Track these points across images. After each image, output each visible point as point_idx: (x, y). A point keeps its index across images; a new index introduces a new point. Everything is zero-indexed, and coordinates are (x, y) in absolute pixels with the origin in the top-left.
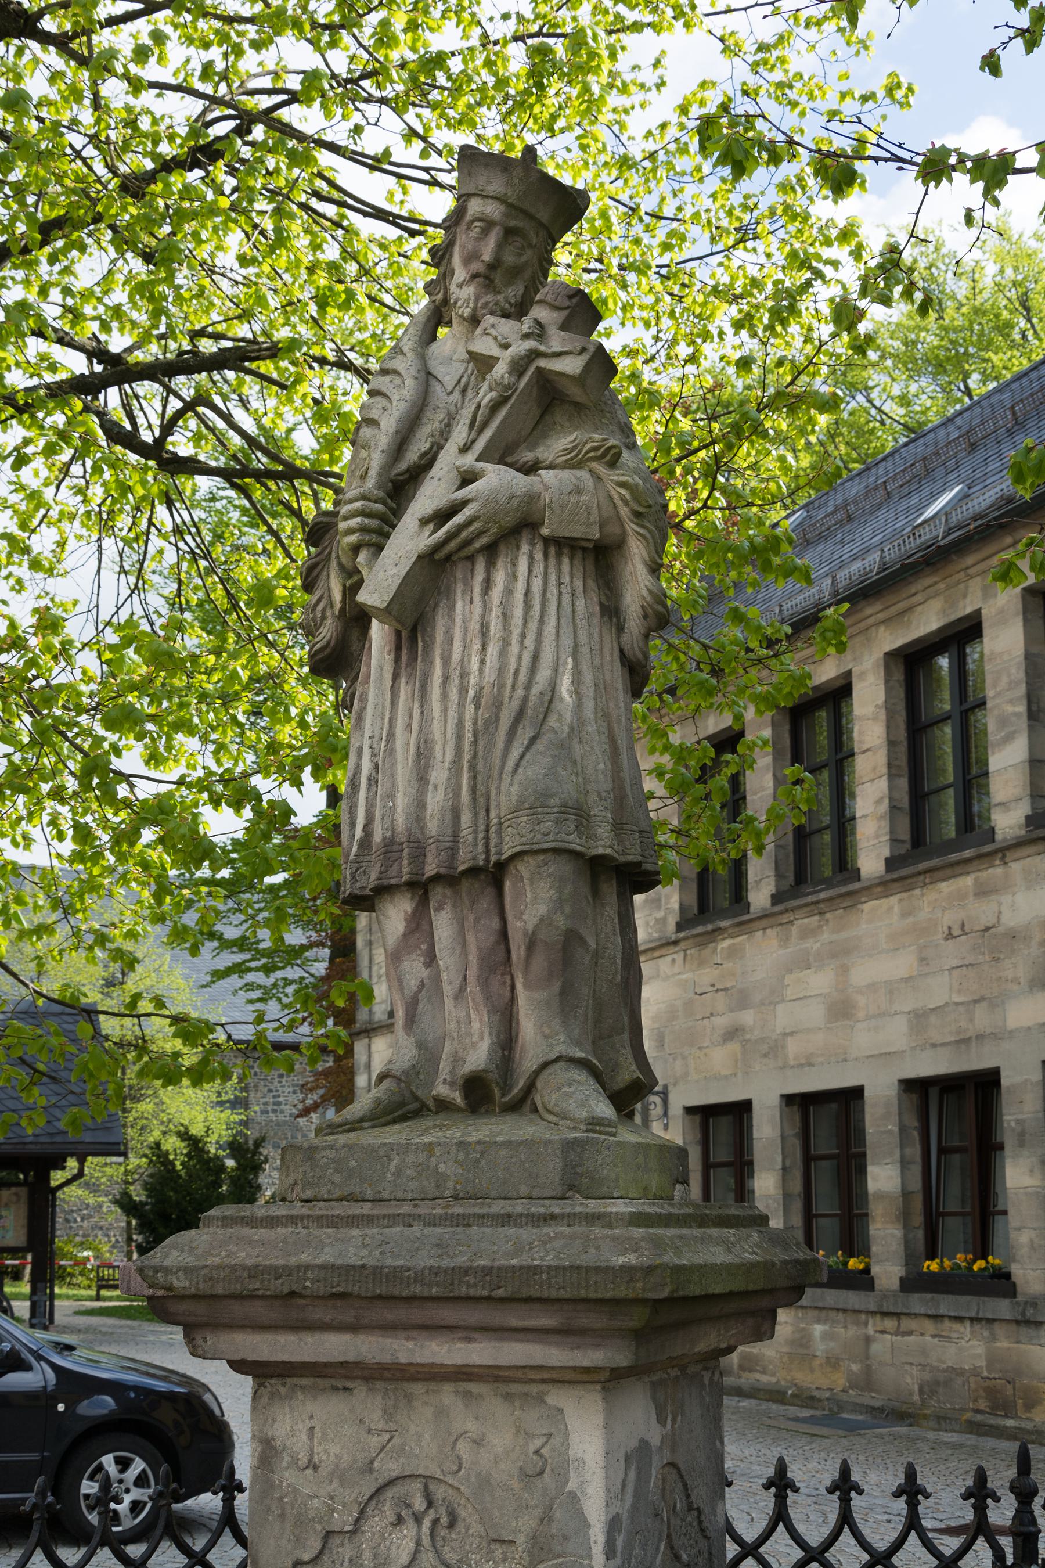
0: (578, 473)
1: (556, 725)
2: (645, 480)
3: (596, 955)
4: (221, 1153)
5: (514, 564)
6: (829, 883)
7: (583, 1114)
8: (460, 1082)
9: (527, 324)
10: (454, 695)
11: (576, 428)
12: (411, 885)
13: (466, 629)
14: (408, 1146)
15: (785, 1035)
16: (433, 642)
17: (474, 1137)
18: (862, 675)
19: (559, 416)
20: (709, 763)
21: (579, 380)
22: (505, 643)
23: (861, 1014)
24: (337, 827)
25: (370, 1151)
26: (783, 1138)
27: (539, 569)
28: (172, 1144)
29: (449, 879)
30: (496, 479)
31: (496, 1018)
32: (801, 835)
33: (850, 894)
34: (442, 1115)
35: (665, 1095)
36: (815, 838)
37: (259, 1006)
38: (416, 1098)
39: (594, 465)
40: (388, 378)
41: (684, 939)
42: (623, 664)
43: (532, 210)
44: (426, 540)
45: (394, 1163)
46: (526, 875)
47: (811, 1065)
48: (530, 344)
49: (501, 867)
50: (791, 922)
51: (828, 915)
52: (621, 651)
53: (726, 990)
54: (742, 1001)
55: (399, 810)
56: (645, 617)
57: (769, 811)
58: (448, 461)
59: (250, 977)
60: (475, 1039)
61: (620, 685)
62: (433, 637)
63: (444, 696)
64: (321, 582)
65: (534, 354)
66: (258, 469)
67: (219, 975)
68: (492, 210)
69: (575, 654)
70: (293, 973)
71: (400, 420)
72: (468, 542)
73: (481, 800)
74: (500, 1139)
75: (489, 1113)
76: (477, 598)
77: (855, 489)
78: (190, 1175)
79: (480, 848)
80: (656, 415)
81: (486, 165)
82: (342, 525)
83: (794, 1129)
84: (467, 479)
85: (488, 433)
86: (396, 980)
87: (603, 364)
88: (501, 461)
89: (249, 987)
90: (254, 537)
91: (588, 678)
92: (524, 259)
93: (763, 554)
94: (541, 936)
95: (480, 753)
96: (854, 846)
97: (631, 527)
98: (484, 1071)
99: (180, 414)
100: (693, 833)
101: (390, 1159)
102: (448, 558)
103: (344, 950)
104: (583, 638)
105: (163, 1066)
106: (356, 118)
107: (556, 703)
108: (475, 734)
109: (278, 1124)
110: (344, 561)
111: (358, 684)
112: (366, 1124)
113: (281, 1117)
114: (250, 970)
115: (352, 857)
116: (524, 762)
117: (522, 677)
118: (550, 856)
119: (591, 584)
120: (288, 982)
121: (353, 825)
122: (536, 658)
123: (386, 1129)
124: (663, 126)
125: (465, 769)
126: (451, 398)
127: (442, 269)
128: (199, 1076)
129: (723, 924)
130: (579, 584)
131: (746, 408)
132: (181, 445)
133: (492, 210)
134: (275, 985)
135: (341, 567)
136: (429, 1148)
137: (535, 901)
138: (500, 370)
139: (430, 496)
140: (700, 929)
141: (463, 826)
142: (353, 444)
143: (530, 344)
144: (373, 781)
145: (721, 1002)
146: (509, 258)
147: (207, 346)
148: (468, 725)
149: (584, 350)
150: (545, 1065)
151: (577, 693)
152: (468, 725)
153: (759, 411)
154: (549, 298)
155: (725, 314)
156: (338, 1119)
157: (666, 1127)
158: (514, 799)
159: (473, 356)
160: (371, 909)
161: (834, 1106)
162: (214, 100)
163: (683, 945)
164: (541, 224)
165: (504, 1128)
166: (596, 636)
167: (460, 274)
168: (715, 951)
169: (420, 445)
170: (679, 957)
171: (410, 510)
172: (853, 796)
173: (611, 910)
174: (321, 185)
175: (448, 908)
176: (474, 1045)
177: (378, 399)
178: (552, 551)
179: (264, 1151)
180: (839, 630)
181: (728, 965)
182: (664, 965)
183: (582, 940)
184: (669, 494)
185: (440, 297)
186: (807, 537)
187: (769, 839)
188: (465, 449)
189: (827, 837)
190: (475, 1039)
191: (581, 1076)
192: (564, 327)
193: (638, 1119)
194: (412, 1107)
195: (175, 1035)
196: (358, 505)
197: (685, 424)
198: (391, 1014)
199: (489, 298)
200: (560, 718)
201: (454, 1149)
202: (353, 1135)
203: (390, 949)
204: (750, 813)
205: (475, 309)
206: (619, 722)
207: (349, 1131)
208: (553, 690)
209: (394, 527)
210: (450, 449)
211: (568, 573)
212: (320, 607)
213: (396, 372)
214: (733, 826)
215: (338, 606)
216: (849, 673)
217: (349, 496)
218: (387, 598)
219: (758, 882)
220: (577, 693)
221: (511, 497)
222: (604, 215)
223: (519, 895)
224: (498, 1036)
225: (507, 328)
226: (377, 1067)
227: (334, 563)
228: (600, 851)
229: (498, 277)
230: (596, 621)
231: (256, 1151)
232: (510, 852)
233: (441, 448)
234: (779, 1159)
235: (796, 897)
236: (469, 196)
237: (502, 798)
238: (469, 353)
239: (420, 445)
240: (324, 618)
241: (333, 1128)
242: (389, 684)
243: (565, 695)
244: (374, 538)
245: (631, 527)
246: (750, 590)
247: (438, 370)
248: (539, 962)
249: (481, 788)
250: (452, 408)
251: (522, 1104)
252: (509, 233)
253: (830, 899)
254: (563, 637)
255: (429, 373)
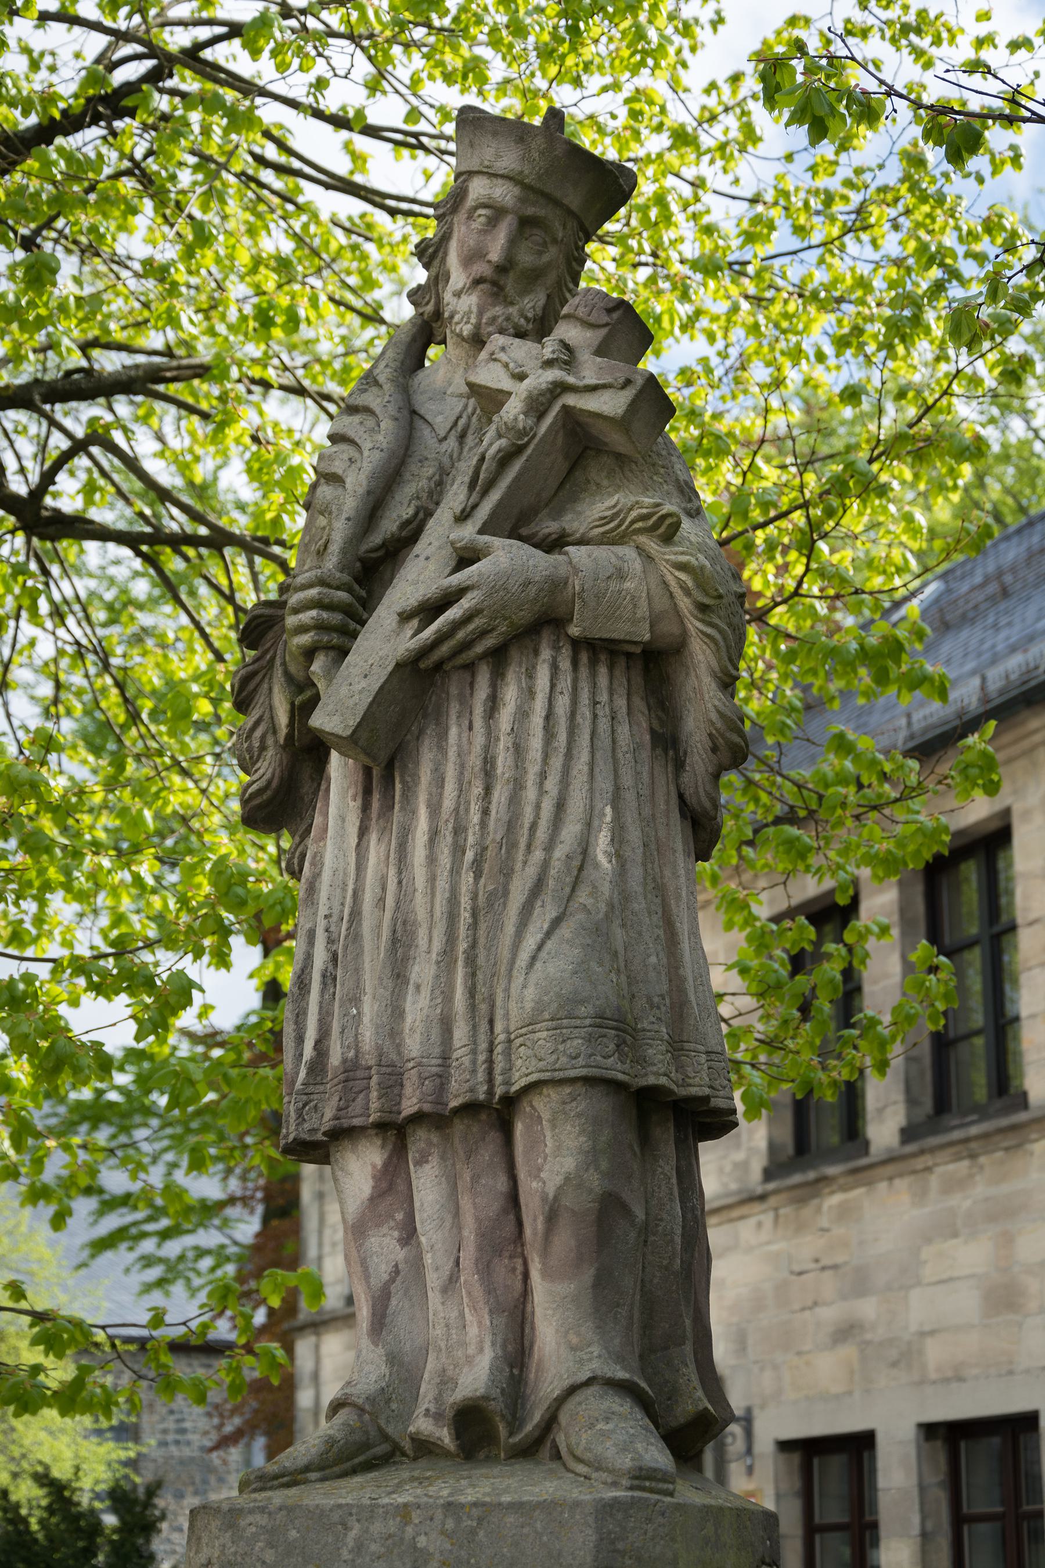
0: (620, 550)
1: (589, 902)
2: (713, 560)
3: (646, 1230)
4: (97, 1505)
5: (531, 675)
6: (983, 1113)
7: (626, 1462)
8: (449, 1413)
9: (549, 348)
10: (445, 858)
11: (618, 488)
12: (382, 1127)
13: (462, 766)
14: (373, 1508)
15: (923, 1334)
16: (416, 783)
17: (469, 1496)
18: (1027, 814)
19: (595, 472)
20: (809, 948)
21: (623, 423)
22: (518, 785)
23: (1033, 1305)
24: (276, 1037)
25: (319, 1515)
26: (922, 1488)
27: (565, 682)
28: (27, 1493)
29: (436, 1119)
30: (506, 558)
31: (502, 1320)
32: (943, 1045)
33: (1014, 1128)
34: (423, 1462)
35: (747, 1421)
36: (963, 1048)
37: (156, 1298)
38: (385, 1437)
39: (642, 539)
40: (356, 419)
41: (775, 1192)
42: (683, 816)
43: (558, 194)
44: (408, 641)
45: (353, 1534)
46: (546, 1115)
47: (960, 1379)
48: (553, 374)
49: (510, 1103)
50: (928, 1169)
51: (982, 1160)
52: (681, 796)
53: (835, 1267)
54: (859, 1284)
55: (366, 1020)
56: (714, 749)
57: (896, 1010)
58: (440, 534)
59: (148, 1246)
60: (471, 1351)
61: (679, 846)
62: (416, 777)
63: (432, 860)
64: (261, 698)
65: (560, 388)
66: (176, 538)
67: (103, 1244)
68: (503, 193)
69: (616, 801)
70: (209, 1238)
71: (372, 477)
72: (466, 645)
73: (483, 1010)
74: (506, 1499)
75: (491, 1459)
76: (478, 723)
77: (1012, 553)
78: (50, 1538)
79: (481, 1076)
80: (727, 464)
81: (495, 134)
82: (291, 621)
83: (937, 1476)
84: (465, 558)
85: (495, 496)
86: (359, 1263)
87: (654, 402)
88: (514, 534)
89: (148, 1261)
90: (168, 620)
91: (634, 835)
92: (546, 258)
93: (883, 659)
94: (566, 1202)
95: (482, 941)
96: (1018, 1054)
97: (694, 625)
98: (485, 1398)
99: (66, 457)
100: (790, 1044)
101: (346, 1528)
102: (439, 666)
103: (282, 1208)
104: (627, 779)
105: (16, 1385)
106: (320, 68)
107: (589, 872)
108: (474, 914)
109: (182, 1462)
110: (293, 669)
111: (309, 841)
112: (313, 1476)
113: (187, 1452)
114: (144, 1235)
115: (298, 1085)
116: (543, 955)
117: (542, 834)
118: (580, 1088)
119: (639, 703)
120: (201, 1253)
121: (300, 1039)
122: (560, 806)
123: (342, 1482)
124: (735, 79)
125: (460, 963)
126: (445, 446)
127: (434, 271)
128: (70, 1399)
129: (831, 1170)
130: (621, 703)
131: (852, 457)
132: (67, 496)
133: (503, 193)
134: (181, 1258)
135: (288, 675)
136: (404, 1511)
137: (556, 1153)
138: (513, 409)
139: (418, 578)
140: (797, 1178)
141: (457, 1043)
142: (307, 507)
143: (553, 374)
144: (329, 979)
145: (829, 1284)
146: (526, 258)
147: (110, 362)
148: (465, 901)
149: (628, 382)
150: (572, 1390)
151: (618, 855)
152: (465, 901)
153: (871, 461)
154: (581, 312)
155: (820, 328)
156: (273, 1468)
157: (750, 1470)
158: (529, 1005)
159: (475, 389)
160: (324, 1159)
161: (996, 1441)
162: (121, 37)
163: (773, 1201)
164: (570, 212)
165: (513, 1482)
166: (646, 777)
167: (458, 278)
168: (819, 1210)
169: (400, 510)
170: (768, 1219)
171: (385, 601)
172: (1015, 982)
173: (667, 1166)
174: (271, 152)
175: (434, 1160)
176: (469, 1360)
177: (343, 447)
178: (584, 657)
179: (160, 1502)
180: (988, 764)
181: (839, 1231)
182: (746, 1230)
183: (625, 1210)
184: (746, 574)
185: (430, 308)
186: (944, 619)
187: (896, 1051)
188: (463, 517)
189: (979, 1042)
190: (471, 1351)
191: (621, 1406)
192: (600, 351)
193: (709, 1472)
194: (381, 1449)
195: (35, 1342)
196: (313, 592)
197: (771, 474)
198: (350, 1300)
199: (498, 310)
200: (595, 892)
201: (439, 1514)
202: (293, 1491)
203: (350, 1219)
204: (870, 1013)
205: (478, 326)
206: (678, 897)
207: (288, 1485)
208: (585, 852)
209: (363, 623)
210: (444, 515)
211: (608, 692)
212: (258, 733)
213: (367, 410)
214: (846, 1032)
215: (283, 731)
216: (1007, 813)
217: (300, 580)
218: (353, 722)
219: (880, 1111)
220: (618, 855)
221: (527, 583)
222: (660, 200)
223: (535, 1143)
224: (504, 1346)
225: (522, 351)
226: (330, 1392)
227: (278, 673)
228: (652, 1080)
229: (510, 284)
230: (645, 754)
231: (148, 1504)
232: (523, 1082)
233: (429, 514)
234: (916, 1519)
235: (935, 1131)
236: (471, 174)
237: (513, 1005)
238: (470, 385)
239: (400, 510)
240: (263, 748)
241: (263, 1481)
242: (353, 840)
243: (602, 859)
244: (335, 639)
245: (694, 625)
246: (861, 701)
247: (427, 408)
248: (564, 1240)
249: (482, 990)
250: (446, 460)
251: (538, 1446)
252: (525, 223)
253: (985, 1136)
254: (599, 778)
255: (414, 412)
